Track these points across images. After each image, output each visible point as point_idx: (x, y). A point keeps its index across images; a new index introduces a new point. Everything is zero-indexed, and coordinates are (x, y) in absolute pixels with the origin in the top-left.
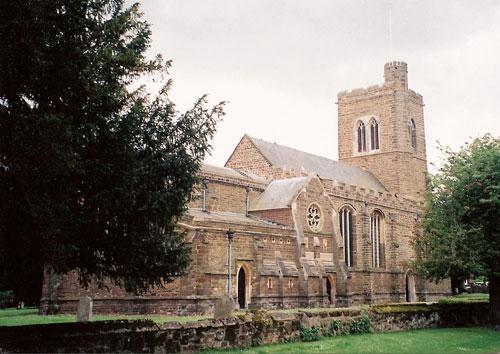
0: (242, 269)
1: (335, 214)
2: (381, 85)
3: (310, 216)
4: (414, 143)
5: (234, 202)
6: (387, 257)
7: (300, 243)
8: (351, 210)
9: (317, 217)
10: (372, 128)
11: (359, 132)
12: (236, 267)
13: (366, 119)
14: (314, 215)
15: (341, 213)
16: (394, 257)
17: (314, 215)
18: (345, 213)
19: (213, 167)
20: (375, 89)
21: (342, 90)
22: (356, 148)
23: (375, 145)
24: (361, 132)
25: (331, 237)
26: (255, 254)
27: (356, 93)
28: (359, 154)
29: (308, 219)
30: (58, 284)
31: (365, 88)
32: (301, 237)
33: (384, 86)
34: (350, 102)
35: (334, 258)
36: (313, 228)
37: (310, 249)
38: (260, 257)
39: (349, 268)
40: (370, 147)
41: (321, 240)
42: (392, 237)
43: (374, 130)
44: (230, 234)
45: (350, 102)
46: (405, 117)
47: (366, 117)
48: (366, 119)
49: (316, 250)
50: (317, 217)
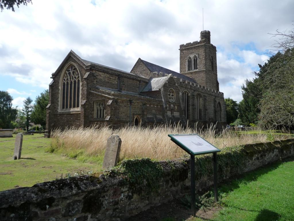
0: (136, 119)
1: (181, 94)
2: (199, 41)
3: (169, 95)
4: (212, 66)
5: (133, 87)
6: (202, 115)
7: (164, 107)
8: (187, 92)
9: (172, 95)
10: (194, 60)
11: (189, 61)
12: (134, 118)
13: (192, 56)
14: (171, 94)
15: (183, 94)
16: (205, 115)
17: (171, 94)
18: (185, 94)
19: (200, 152)
20: (196, 43)
21: (182, 44)
22: (187, 69)
23: (196, 68)
24: (190, 62)
25: (179, 106)
26: (143, 112)
27: (189, 44)
28: (189, 72)
29: (168, 96)
30: (53, 124)
31: (192, 42)
32: (165, 104)
33: (200, 41)
34: (185, 49)
35: (180, 114)
36: (171, 100)
37: (169, 110)
38: (145, 113)
39: (77, 81)
40: (194, 68)
41: (174, 106)
42: (205, 106)
43: (195, 61)
44: (131, 102)
45: (185, 49)
46: (209, 55)
47: (192, 55)
48: (192, 56)
49: (172, 110)
50: (172, 95)
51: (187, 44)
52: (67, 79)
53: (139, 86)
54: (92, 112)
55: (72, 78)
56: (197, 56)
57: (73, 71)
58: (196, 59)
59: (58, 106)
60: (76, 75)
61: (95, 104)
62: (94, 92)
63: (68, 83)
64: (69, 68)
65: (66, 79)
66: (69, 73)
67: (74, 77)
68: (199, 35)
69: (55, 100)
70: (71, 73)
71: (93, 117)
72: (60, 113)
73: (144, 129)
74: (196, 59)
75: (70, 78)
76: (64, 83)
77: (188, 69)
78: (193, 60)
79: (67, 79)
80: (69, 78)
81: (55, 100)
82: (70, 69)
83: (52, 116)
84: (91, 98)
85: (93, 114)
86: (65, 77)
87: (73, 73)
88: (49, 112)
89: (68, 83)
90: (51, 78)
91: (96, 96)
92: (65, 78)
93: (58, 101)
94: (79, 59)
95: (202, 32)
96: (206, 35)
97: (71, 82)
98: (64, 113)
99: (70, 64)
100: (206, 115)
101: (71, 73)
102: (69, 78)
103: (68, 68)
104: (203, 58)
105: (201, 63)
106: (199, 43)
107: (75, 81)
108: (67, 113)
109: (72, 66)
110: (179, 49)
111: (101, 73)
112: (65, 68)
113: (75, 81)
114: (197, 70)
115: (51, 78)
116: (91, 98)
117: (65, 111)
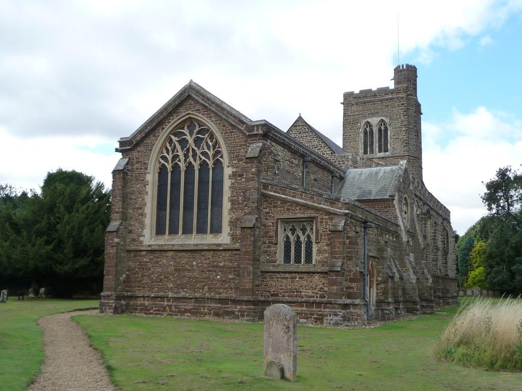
10: (380, 130)
11: (365, 133)
13: (374, 121)
20: (385, 91)
21: (349, 90)
23: (383, 147)
24: (368, 134)
27: (366, 93)
30: (124, 276)
40: (377, 150)
43: (383, 133)
48: (374, 121)
51: (361, 92)
52: (175, 157)
53: (332, 186)
54: (269, 247)
55: (191, 154)
56: (387, 120)
57: (194, 136)
58: (383, 128)
59: (143, 226)
60: (205, 147)
61: (281, 227)
62: (278, 195)
63: (176, 167)
64: (183, 128)
65: (170, 157)
66: (183, 142)
67: (198, 152)
68: (392, 75)
69: (131, 211)
70: (191, 140)
71: (275, 262)
72: (149, 246)
73: (483, 300)
74: (383, 128)
75: (186, 156)
76: (163, 169)
77: (363, 151)
78: (375, 130)
79: (175, 157)
80: (181, 154)
81: (131, 211)
82: (186, 131)
83: (123, 255)
84: (267, 210)
85: (276, 253)
86: (165, 151)
87: (198, 141)
88: (83, 237)
89: (176, 167)
90: (117, 150)
91: (283, 207)
92: (165, 154)
93: (143, 215)
94: (224, 106)
95: (399, 67)
96: (407, 76)
97: (190, 167)
98: (166, 248)
99: (187, 116)
100: (437, 261)
101: (191, 140)
102: (181, 154)
103: (181, 125)
104: (404, 129)
105: (398, 138)
106: (392, 92)
107: (204, 165)
108: (176, 248)
109: (190, 122)
110: (342, 102)
111: (279, 148)
112: (168, 127)
113: (204, 165)
114: (387, 153)
115: (117, 150)
116: (267, 210)
117: (166, 240)
